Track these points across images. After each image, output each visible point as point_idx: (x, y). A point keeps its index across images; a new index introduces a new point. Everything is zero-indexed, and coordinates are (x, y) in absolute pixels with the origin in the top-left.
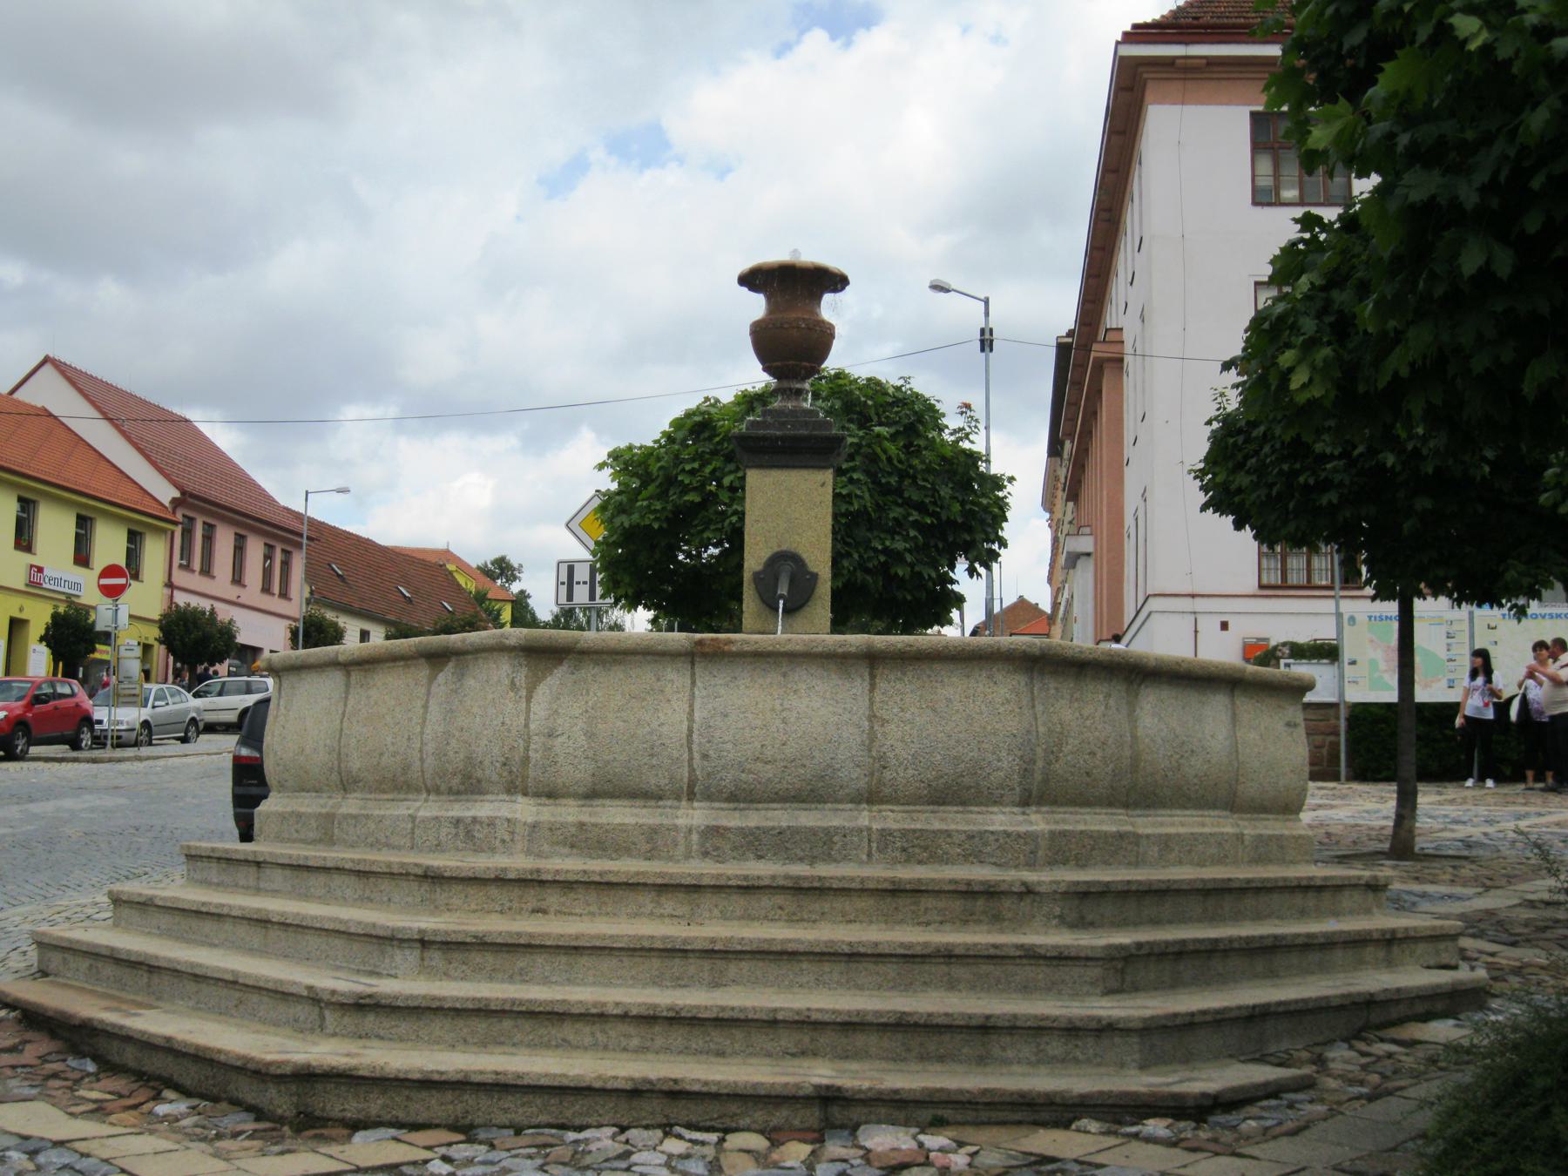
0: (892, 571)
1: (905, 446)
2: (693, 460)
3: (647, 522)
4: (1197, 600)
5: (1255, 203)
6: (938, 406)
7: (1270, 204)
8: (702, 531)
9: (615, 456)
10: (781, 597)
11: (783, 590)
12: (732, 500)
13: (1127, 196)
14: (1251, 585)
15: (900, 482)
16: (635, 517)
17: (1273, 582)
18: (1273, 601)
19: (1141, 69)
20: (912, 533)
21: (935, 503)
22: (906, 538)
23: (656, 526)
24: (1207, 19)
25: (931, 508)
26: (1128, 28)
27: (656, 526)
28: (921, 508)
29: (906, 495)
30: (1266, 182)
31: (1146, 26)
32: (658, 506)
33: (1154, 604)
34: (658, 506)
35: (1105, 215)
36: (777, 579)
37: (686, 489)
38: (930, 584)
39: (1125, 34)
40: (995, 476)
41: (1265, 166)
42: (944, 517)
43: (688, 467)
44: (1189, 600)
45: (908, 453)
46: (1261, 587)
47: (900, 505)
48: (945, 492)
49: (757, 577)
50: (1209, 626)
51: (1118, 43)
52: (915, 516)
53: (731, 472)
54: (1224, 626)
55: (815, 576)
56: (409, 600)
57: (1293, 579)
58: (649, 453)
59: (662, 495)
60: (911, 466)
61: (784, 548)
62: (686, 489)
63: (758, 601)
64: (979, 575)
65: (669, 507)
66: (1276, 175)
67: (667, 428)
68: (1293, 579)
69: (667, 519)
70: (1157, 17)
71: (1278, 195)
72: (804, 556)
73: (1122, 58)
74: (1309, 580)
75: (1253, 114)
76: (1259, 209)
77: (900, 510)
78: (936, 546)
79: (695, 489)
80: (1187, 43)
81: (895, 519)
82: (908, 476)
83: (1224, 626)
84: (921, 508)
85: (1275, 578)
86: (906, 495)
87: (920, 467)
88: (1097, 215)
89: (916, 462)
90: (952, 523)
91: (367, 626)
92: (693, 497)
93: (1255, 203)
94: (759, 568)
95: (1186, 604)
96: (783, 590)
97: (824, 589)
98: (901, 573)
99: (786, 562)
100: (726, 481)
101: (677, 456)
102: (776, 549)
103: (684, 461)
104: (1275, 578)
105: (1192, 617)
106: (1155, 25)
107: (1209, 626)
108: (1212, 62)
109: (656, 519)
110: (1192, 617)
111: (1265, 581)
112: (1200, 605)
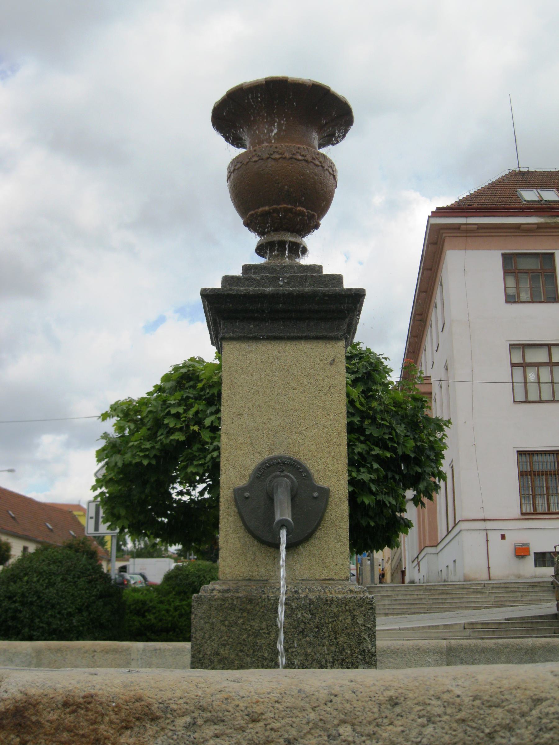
0: (359, 500)
1: (363, 392)
2: (179, 405)
3: (137, 460)
4: (487, 523)
5: (507, 302)
6: (385, 363)
7: (515, 302)
8: (186, 467)
9: (116, 409)
10: (283, 524)
11: (283, 512)
12: (213, 439)
13: (432, 304)
14: (516, 513)
15: (362, 422)
16: (128, 457)
17: (528, 511)
18: (530, 522)
19: (442, 231)
20: (376, 466)
21: (391, 439)
22: (371, 470)
23: (145, 462)
24: (476, 205)
25: (390, 444)
26: (434, 210)
27: (145, 462)
28: (381, 443)
29: (367, 432)
30: (512, 291)
31: (443, 208)
32: (148, 445)
33: (463, 526)
34: (148, 445)
35: (418, 317)
36: (270, 499)
37: (171, 431)
38: (148, 533)
39: (433, 212)
40: (437, 419)
41: (511, 282)
42: (400, 452)
43: (173, 411)
44: (483, 523)
45: (367, 397)
46: (522, 514)
47: (362, 442)
48: (401, 430)
49: (239, 495)
50: (495, 537)
51: (429, 217)
52: (376, 451)
53: (212, 414)
54: (503, 537)
55: (325, 493)
56: (51, 530)
57: (540, 509)
58: (143, 402)
59: (152, 437)
60: (370, 408)
61: (278, 452)
62: (171, 431)
63: (242, 532)
64: (423, 504)
65: (158, 446)
66: (518, 287)
67: (159, 383)
68: (540, 509)
69: (155, 456)
70: (449, 205)
71: (519, 297)
72: (308, 464)
73: (432, 225)
74: (549, 509)
75: (503, 255)
76: (509, 305)
77: (363, 446)
78: (393, 478)
79: (181, 429)
80: (466, 217)
81: (360, 454)
82: (368, 417)
83: (503, 537)
84: (381, 443)
85: (529, 509)
86: (367, 432)
87: (379, 408)
88: (414, 317)
89: (375, 404)
90: (405, 458)
91: (27, 544)
92: (179, 437)
93: (507, 302)
94: (243, 482)
95: (480, 525)
96: (283, 512)
97: (339, 512)
98: (367, 501)
99: (281, 470)
100: (207, 422)
101: (164, 401)
102: (267, 455)
103: (170, 405)
104: (529, 509)
105: (485, 533)
106: (447, 208)
107: (495, 537)
108: (481, 227)
109: (146, 457)
110: (485, 533)
111: (524, 511)
112: (489, 525)
